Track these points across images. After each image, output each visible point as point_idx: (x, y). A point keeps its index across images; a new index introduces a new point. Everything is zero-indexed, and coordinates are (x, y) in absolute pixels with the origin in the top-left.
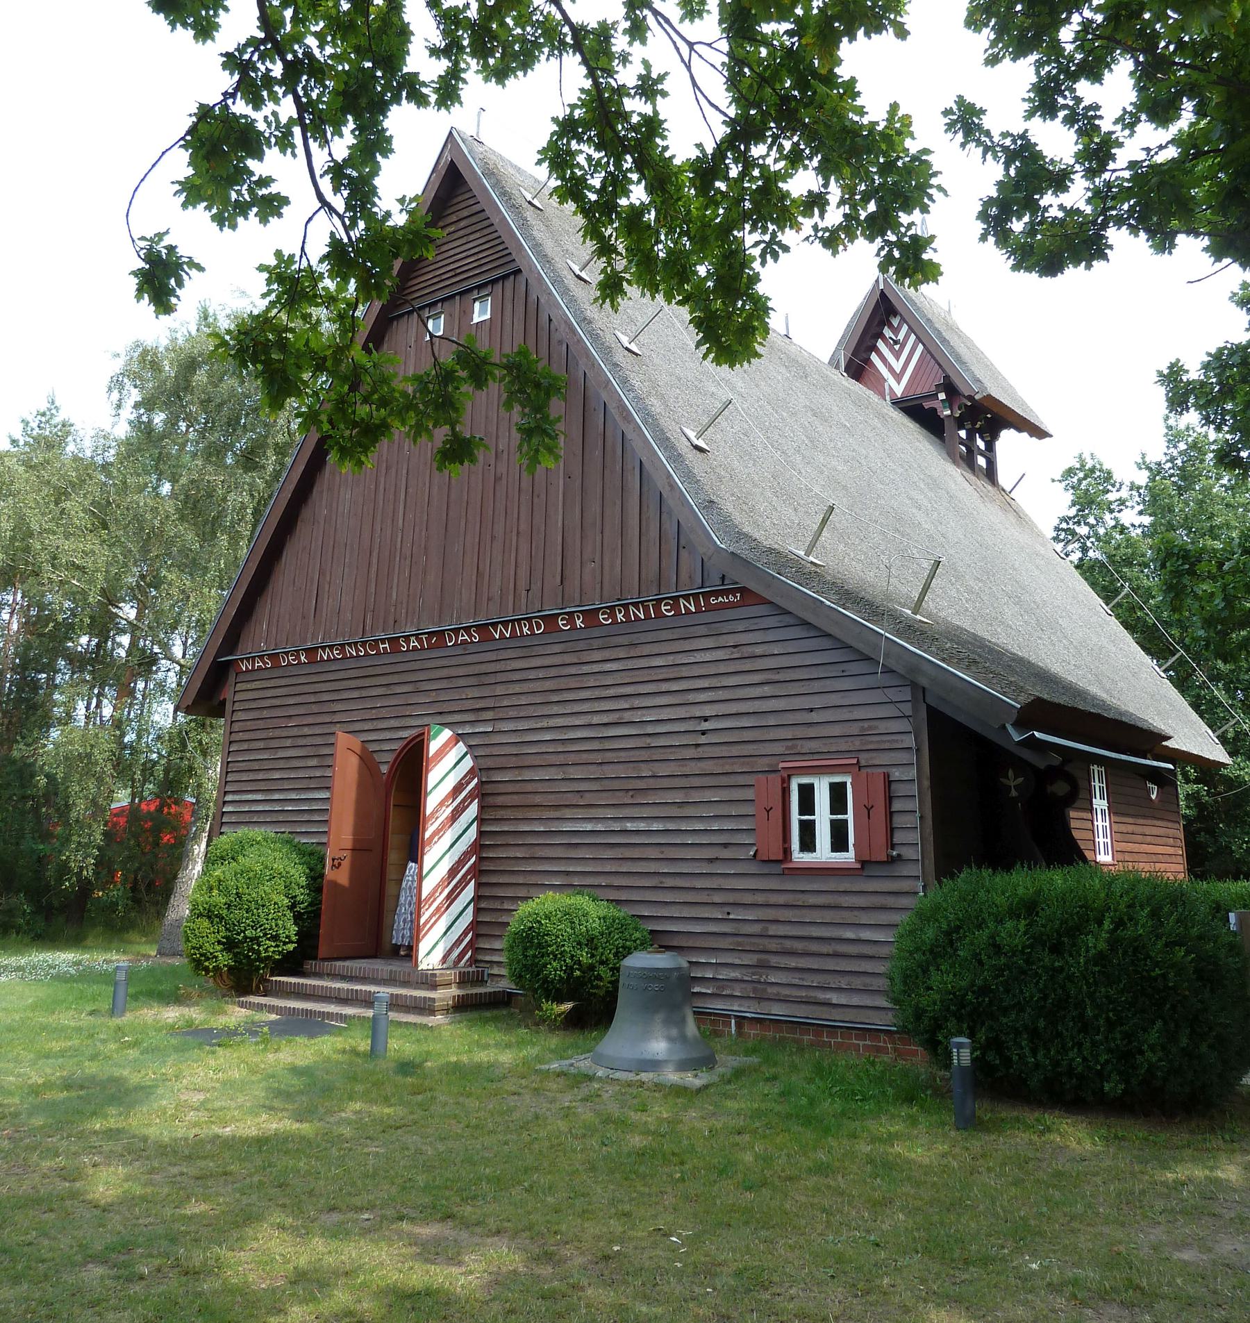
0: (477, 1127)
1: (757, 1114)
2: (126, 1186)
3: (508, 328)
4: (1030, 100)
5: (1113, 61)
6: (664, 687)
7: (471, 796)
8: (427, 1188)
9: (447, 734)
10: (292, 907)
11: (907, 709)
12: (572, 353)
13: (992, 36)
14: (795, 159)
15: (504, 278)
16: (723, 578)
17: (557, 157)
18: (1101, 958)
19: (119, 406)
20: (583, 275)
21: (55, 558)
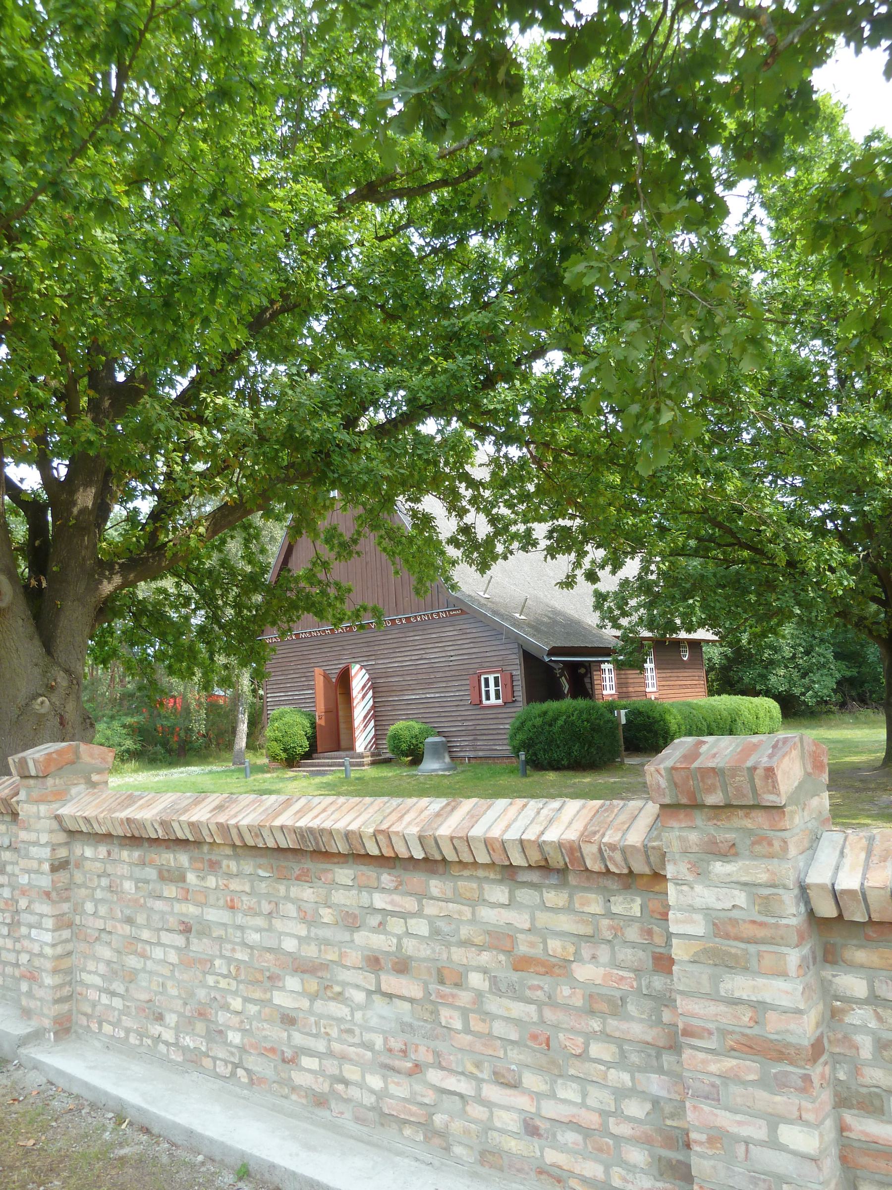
7: (369, 689)
9: (358, 666)
11: (516, 651)
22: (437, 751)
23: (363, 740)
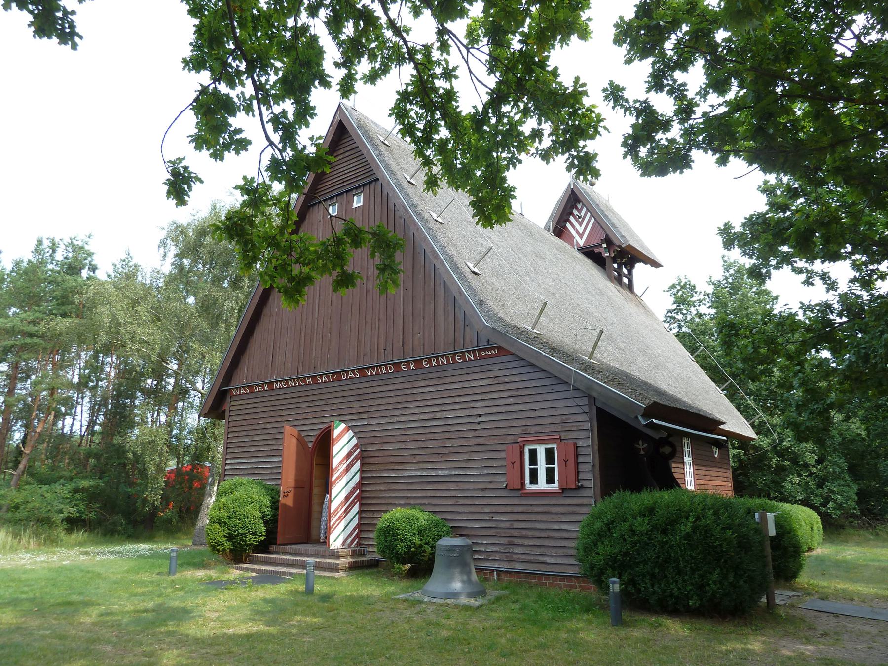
0: (361, 627)
1: (507, 619)
2: (178, 659)
3: (372, 210)
4: (649, 82)
5: (695, 59)
6: (458, 399)
7: (356, 459)
8: (335, 658)
10: (263, 518)
12: (406, 223)
13: (628, 48)
14: (526, 113)
15: (370, 183)
16: (488, 341)
17: (400, 113)
18: (688, 536)
19: (165, 256)
20: (412, 181)
21: (133, 337)
22: (460, 559)
23: (338, 536)
